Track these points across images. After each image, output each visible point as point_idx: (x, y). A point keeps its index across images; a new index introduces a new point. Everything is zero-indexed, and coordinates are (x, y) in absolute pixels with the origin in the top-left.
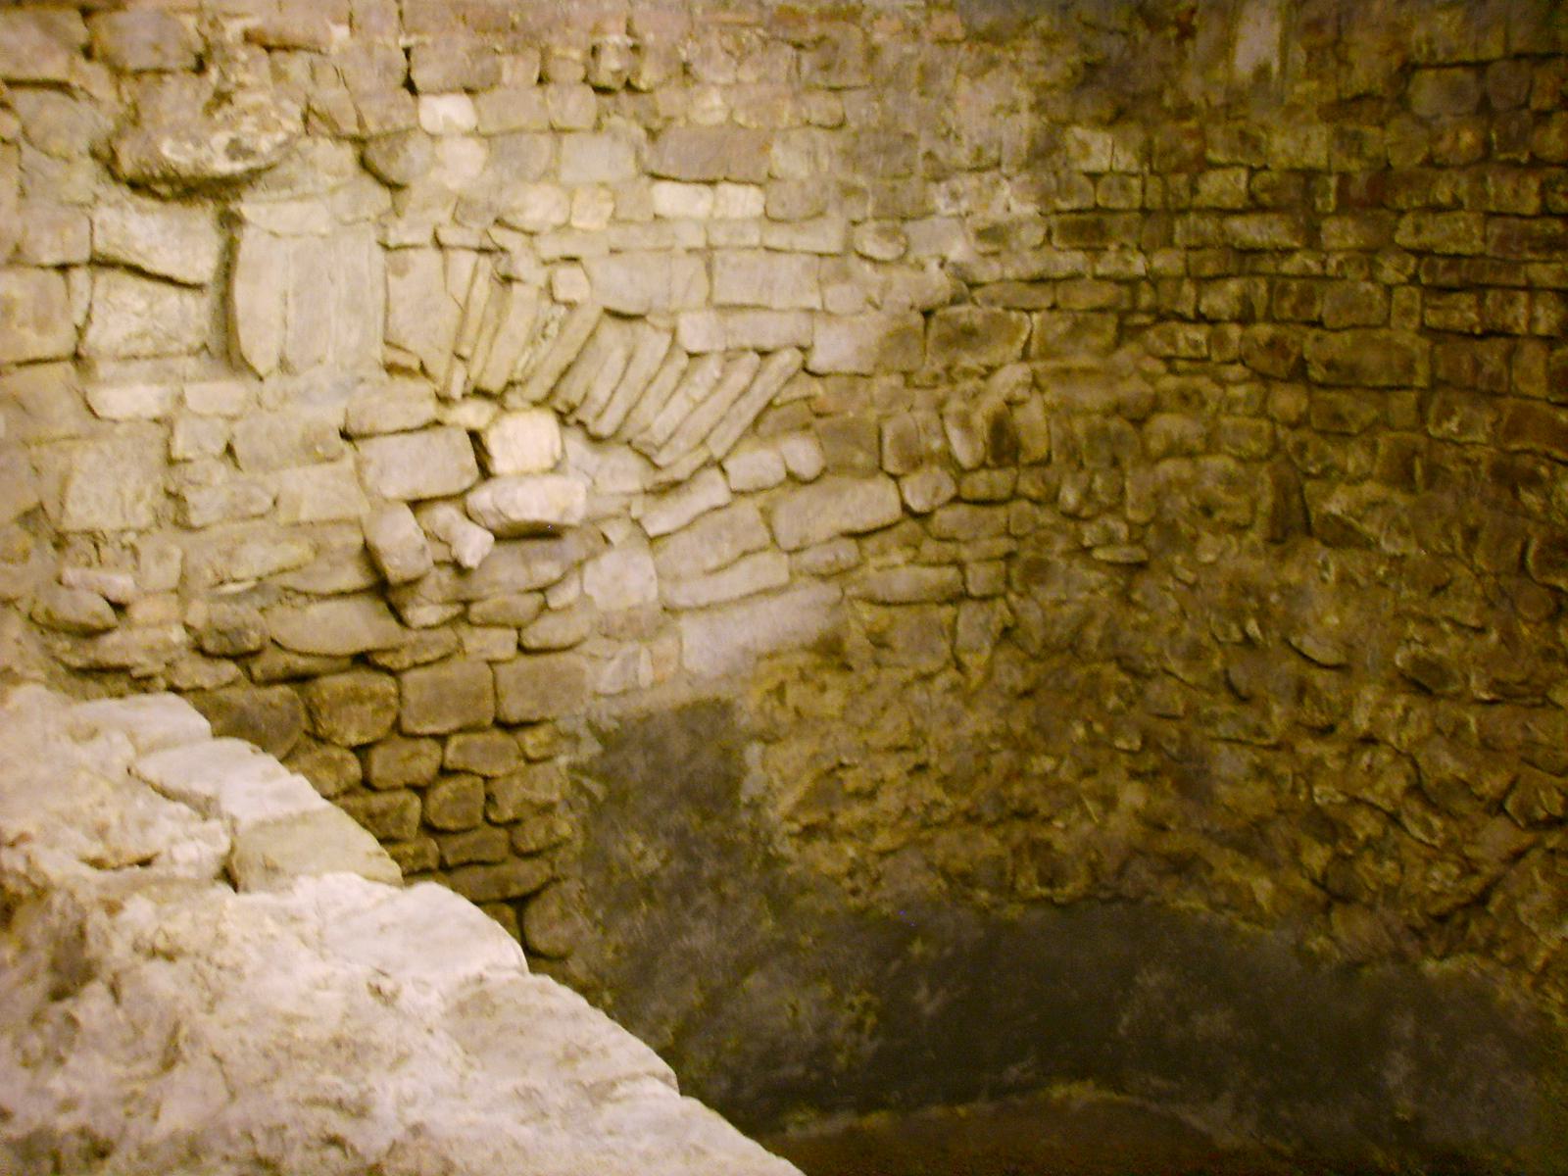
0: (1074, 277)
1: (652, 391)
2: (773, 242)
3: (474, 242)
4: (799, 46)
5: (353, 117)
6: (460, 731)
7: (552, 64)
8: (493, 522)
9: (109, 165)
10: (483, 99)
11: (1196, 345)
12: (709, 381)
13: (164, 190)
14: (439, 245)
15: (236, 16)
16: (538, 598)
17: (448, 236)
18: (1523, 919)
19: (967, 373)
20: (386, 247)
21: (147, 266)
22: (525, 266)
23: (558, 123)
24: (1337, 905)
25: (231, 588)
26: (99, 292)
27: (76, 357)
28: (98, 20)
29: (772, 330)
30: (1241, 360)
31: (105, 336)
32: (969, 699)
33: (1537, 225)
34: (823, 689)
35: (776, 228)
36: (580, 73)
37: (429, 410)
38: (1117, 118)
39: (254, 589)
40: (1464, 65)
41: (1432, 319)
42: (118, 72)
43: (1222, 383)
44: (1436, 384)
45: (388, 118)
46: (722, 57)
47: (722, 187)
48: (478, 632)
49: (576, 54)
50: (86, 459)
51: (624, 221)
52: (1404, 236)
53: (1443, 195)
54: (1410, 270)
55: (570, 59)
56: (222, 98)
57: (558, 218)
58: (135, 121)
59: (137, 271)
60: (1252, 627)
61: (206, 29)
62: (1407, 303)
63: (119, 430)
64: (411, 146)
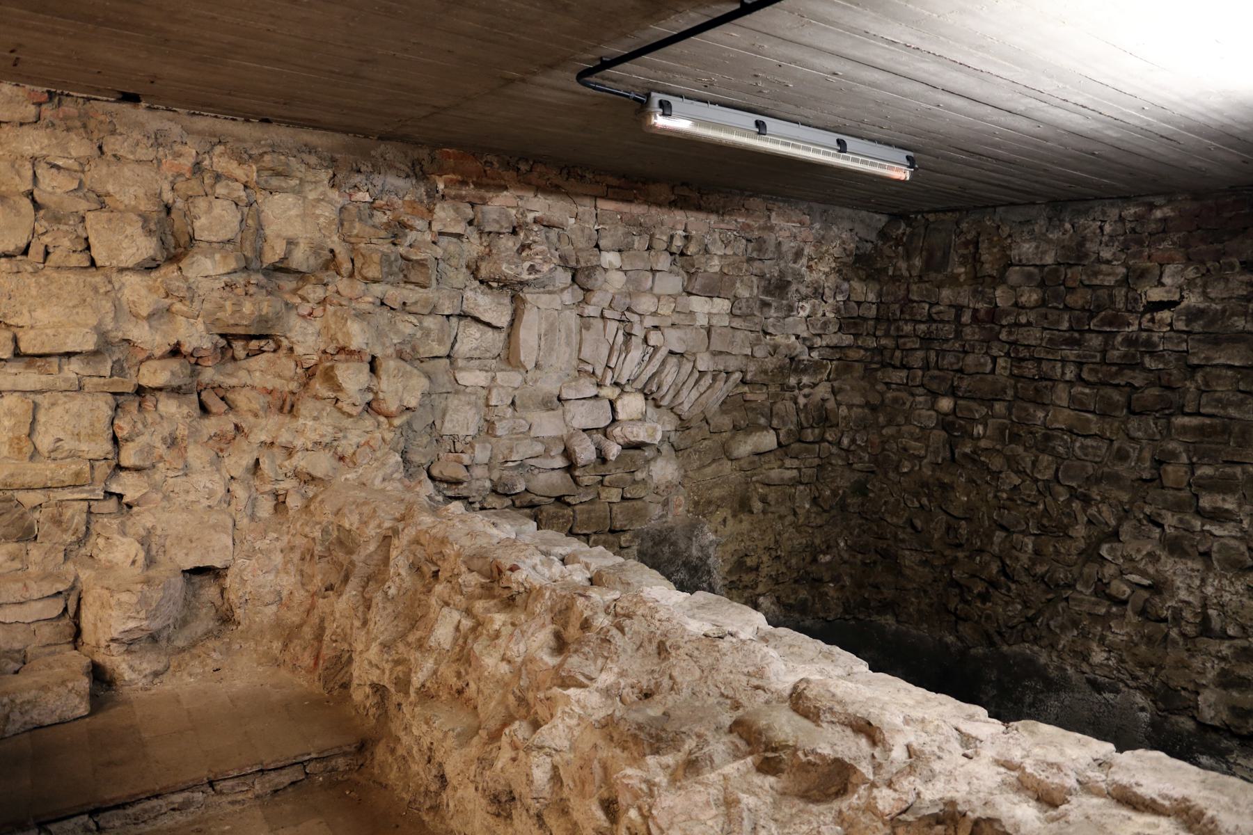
0: (849, 347)
1: (685, 387)
2: (734, 325)
3: (618, 317)
4: (749, 241)
5: (574, 258)
6: (595, 533)
7: (655, 241)
8: (621, 441)
9: (474, 272)
10: (625, 254)
11: (901, 378)
12: (708, 384)
13: (495, 285)
14: (602, 317)
15: (532, 211)
16: (600, 478)
17: (607, 314)
18: (1052, 627)
19: (805, 386)
20: (581, 316)
21: (482, 318)
22: (638, 331)
23: (655, 268)
24: (961, 622)
25: (510, 464)
26: (461, 329)
27: (449, 356)
28: (478, 208)
29: (733, 364)
30: (922, 385)
31: (463, 348)
32: (798, 528)
33: (1067, 335)
34: (741, 521)
35: (736, 319)
36: (665, 246)
37: (593, 391)
38: (867, 278)
39: (519, 465)
40: (1035, 266)
41: (1016, 372)
42: (481, 233)
43: (913, 395)
44: (1016, 397)
45: (589, 260)
46: (720, 243)
47: (715, 299)
48: (607, 490)
49: (665, 238)
50: (454, 402)
51: (678, 312)
52: (1003, 336)
53: (1023, 320)
54: (1006, 351)
55: (661, 243)
56: (524, 247)
57: (653, 309)
58: (490, 254)
59: (477, 320)
60: (925, 501)
61: (519, 216)
62: (1004, 365)
63: (468, 390)
64: (597, 273)
